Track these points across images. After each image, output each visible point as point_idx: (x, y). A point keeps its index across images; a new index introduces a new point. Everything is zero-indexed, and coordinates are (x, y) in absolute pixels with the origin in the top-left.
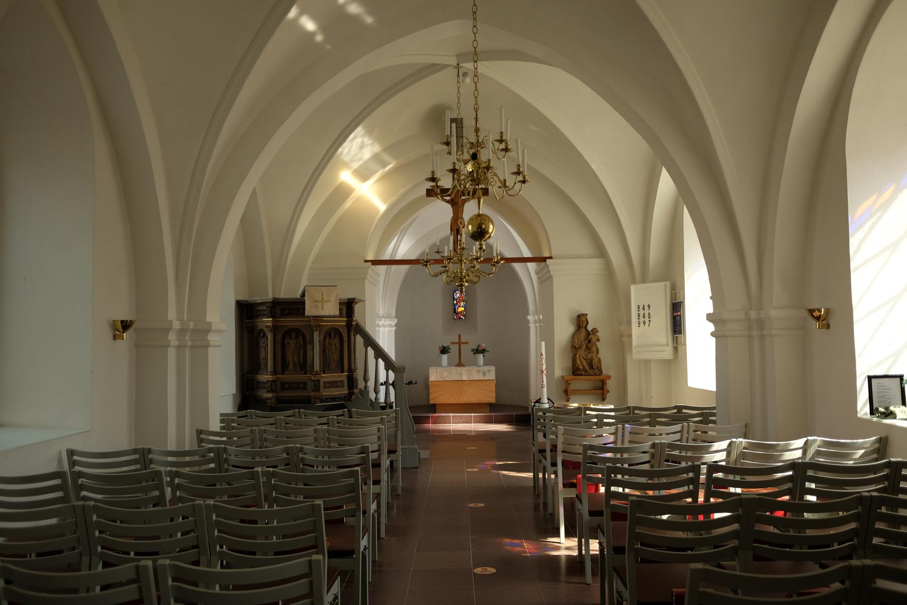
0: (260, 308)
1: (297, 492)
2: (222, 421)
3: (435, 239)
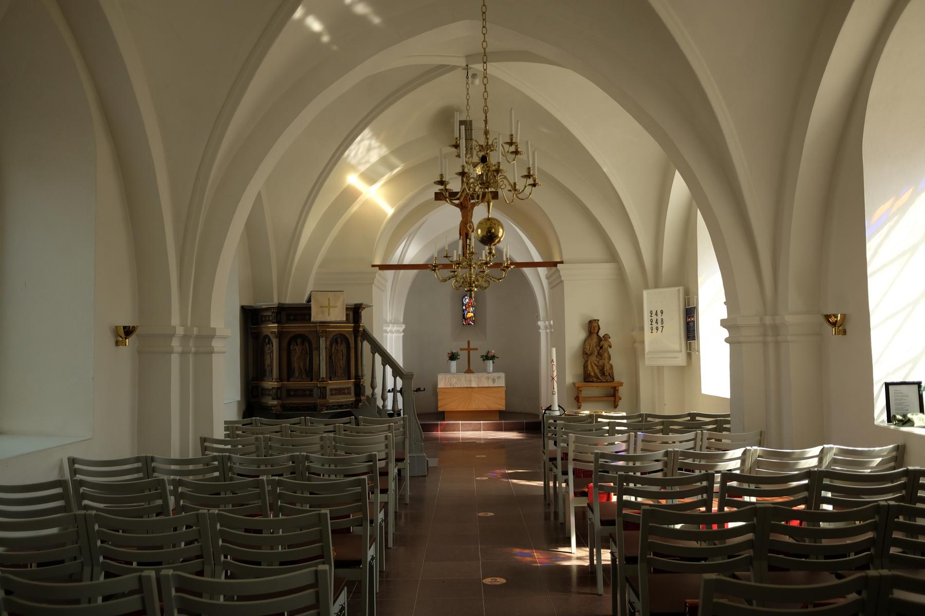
0: (265, 314)
1: (303, 501)
2: (226, 429)
3: (444, 243)
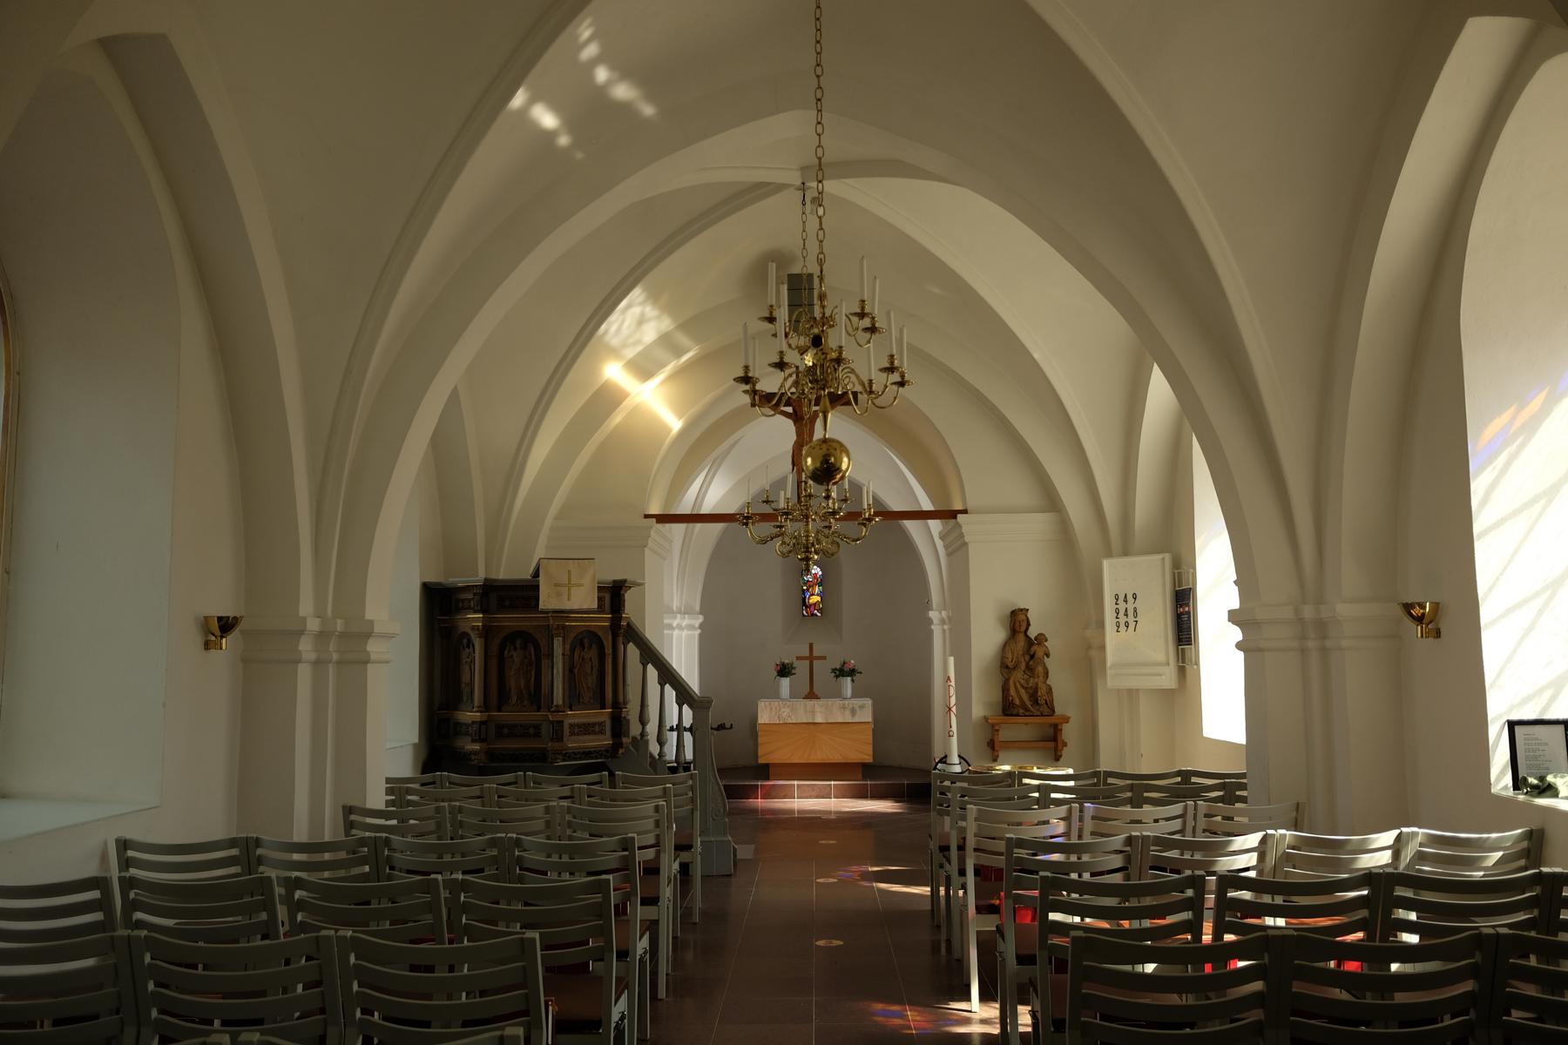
1: (511, 917)
2: (389, 791)
3: (763, 482)
